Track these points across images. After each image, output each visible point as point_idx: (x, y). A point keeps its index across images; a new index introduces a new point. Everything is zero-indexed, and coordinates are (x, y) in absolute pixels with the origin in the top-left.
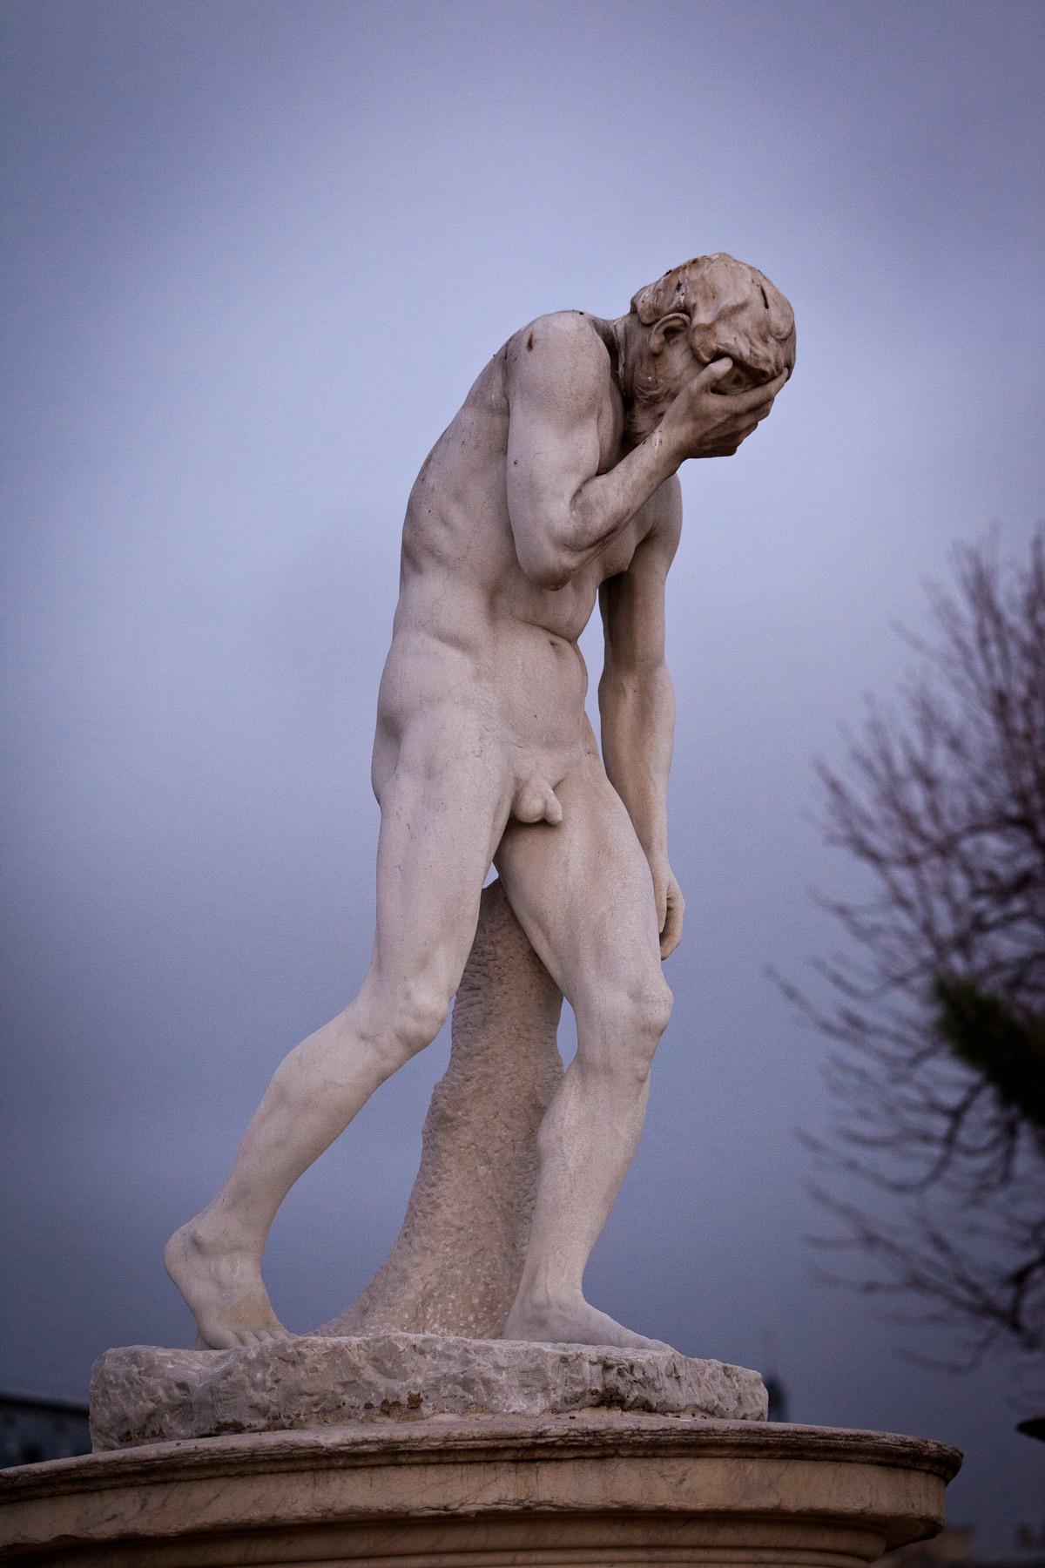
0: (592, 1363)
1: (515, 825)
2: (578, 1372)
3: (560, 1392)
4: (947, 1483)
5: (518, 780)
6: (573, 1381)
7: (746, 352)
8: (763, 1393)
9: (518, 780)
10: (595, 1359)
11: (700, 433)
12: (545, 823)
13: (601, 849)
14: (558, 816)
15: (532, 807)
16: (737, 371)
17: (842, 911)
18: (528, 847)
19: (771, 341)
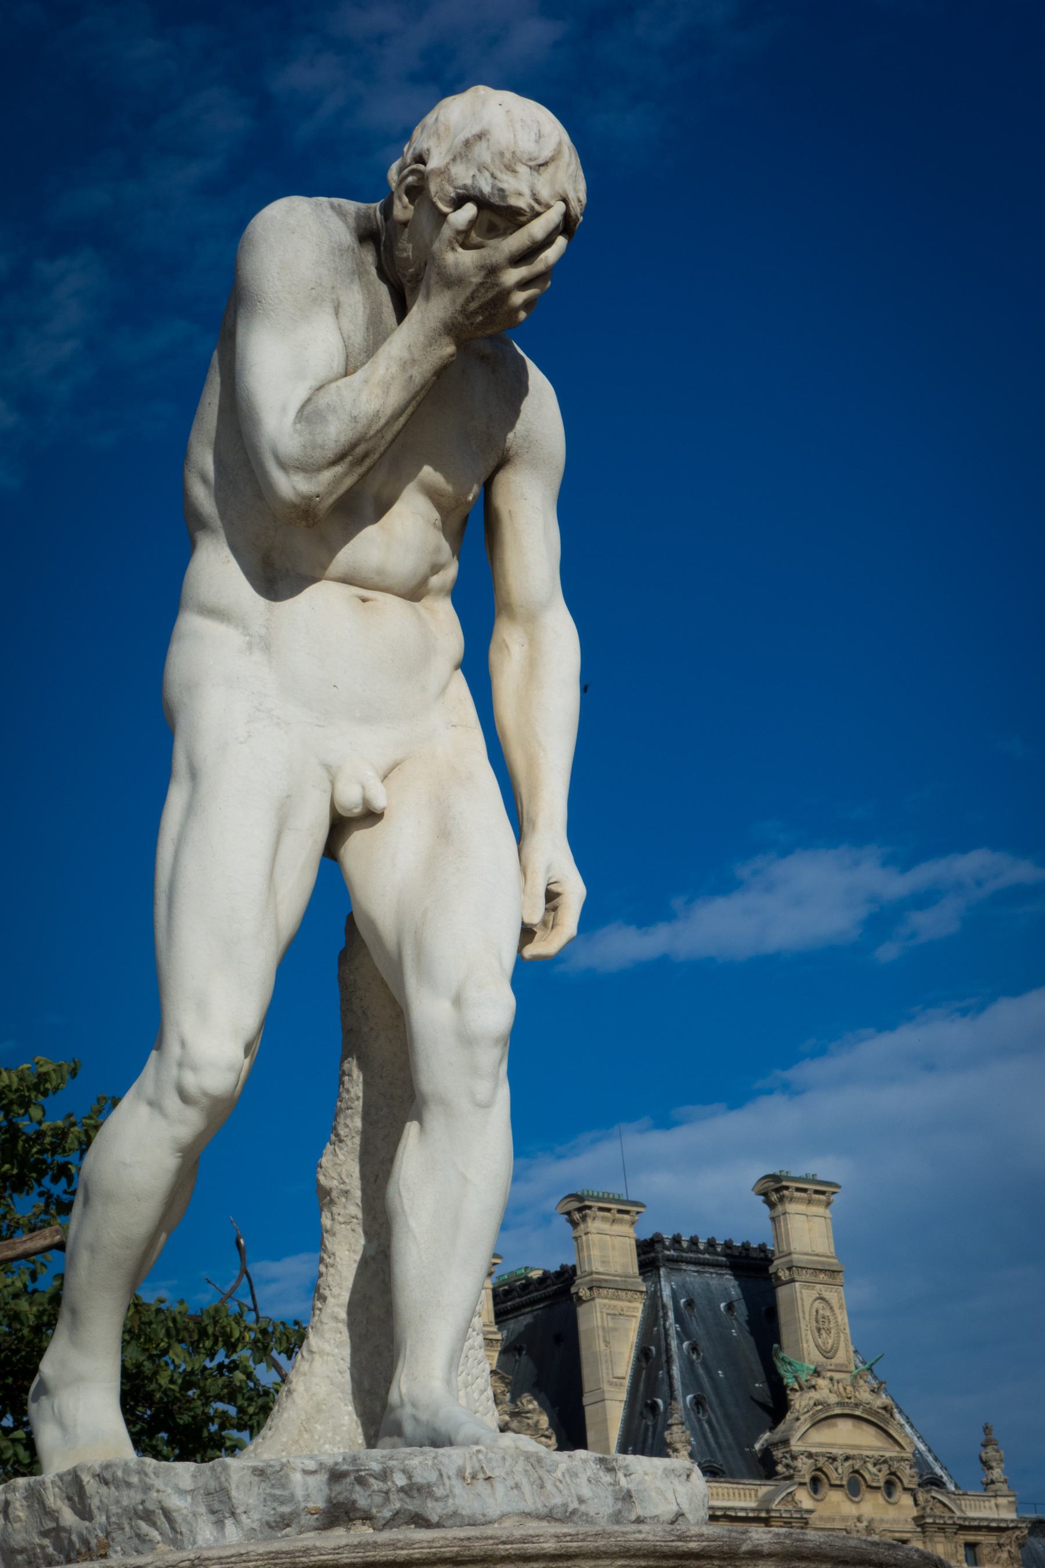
0: (306, 1472)
1: (340, 826)
2: (283, 1487)
3: (255, 1516)
4: (283, 1466)
5: (327, 768)
6: (275, 1498)
7: (487, 189)
8: (147, 1320)
9: (327, 768)
10: (311, 1465)
11: (460, 301)
12: (371, 816)
13: (444, 832)
14: (379, 802)
15: (350, 798)
16: (487, 215)
17: (337, 314)
18: (357, 845)
19: (522, 169)
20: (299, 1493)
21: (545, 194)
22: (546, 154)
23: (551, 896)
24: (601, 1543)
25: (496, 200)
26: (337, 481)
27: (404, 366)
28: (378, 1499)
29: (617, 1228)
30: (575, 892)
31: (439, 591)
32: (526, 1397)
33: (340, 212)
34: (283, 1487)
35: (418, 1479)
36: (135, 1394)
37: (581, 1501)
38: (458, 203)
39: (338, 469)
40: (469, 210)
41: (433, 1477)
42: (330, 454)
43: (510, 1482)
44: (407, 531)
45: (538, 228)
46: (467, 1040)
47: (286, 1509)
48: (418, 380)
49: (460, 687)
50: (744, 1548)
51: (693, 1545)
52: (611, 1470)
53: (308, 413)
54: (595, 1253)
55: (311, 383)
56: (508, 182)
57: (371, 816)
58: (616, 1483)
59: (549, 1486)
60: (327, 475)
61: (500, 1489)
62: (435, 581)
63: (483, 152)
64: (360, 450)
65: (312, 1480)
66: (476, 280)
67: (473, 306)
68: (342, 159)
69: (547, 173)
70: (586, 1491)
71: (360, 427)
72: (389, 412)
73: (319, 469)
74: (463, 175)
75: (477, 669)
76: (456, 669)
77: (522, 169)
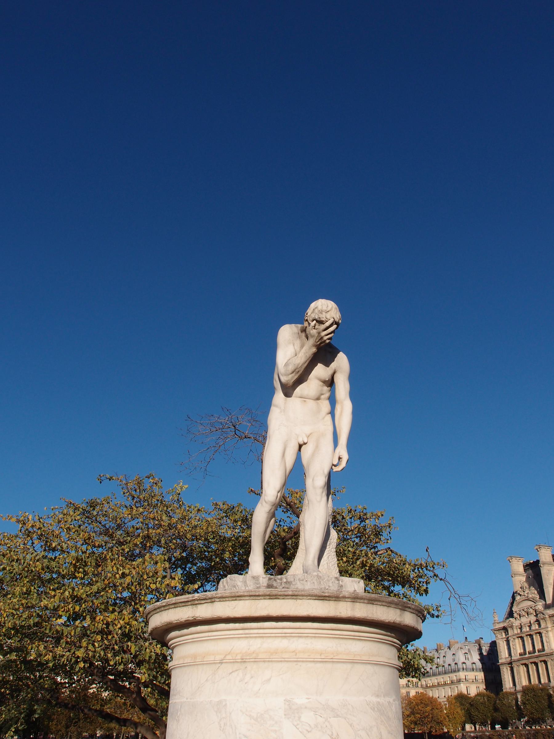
1: (300, 446)
3: (252, 587)
19: (324, 313)
20: (261, 583)
21: (328, 317)
22: (329, 309)
23: (340, 458)
24: (303, 593)
25: (318, 319)
26: (293, 377)
27: (305, 354)
28: (279, 584)
29: (547, 552)
30: (345, 457)
31: (324, 399)
32: (532, 587)
33: (297, 327)
34: (258, 581)
35: (289, 580)
36: (266, 563)
37: (329, 587)
38: (313, 320)
39: (293, 375)
40: (315, 322)
41: (292, 580)
42: (290, 372)
43: (312, 582)
44: (312, 386)
45: (327, 324)
46: (314, 488)
47: (258, 586)
48: (308, 356)
49: (329, 417)
50: (341, 596)
51: (327, 594)
52: (338, 580)
53: (286, 365)
54: (543, 557)
55: (288, 359)
56: (321, 316)
57: (305, 444)
58: (339, 583)
59: (322, 583)
60: (291, 376)
61: (309, 583)
62: (322, 397)
63: (316, 311)
64: (297, 370)
65: (264, 580)
66: (317, 335)
67: (317, 340)
68: (297, 316)
69: (329, 313)
70: (331, 585)
71: (296, 366)
72: (302, 363)
73: (289, 375)
74: (313, 316)
75: (332, 413)
76: (328, 414)
77: (324, 313)
